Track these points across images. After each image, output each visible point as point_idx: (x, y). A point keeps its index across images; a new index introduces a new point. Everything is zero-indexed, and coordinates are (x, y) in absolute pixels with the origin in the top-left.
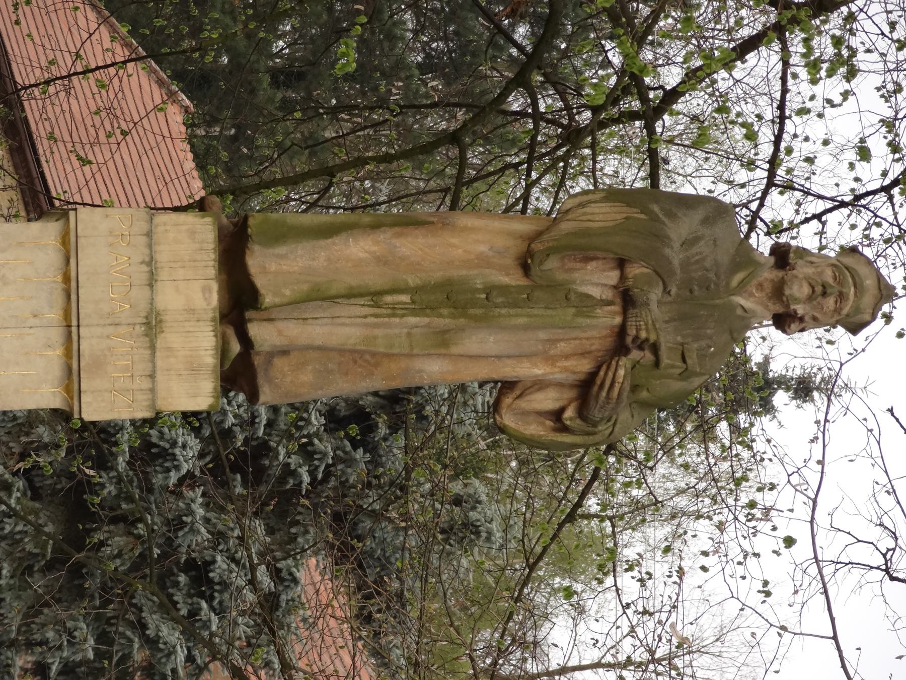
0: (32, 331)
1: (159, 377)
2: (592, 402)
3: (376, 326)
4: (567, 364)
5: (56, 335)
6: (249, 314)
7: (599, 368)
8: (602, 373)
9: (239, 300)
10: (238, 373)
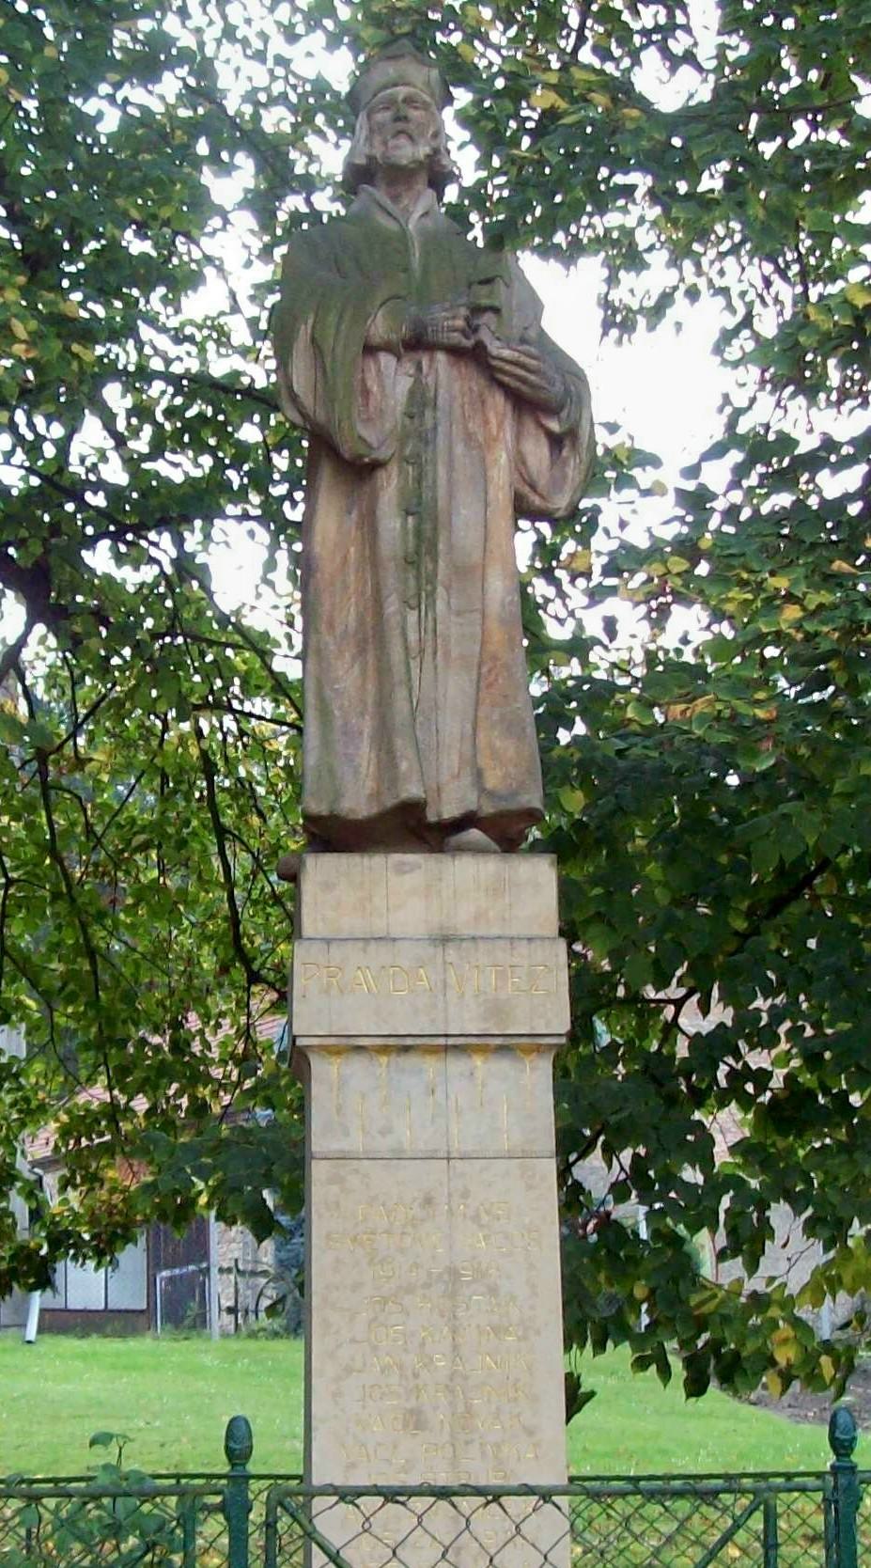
0: (452, 1097)
1: (514, 933)
2: (542, 395)
3: (447, 654)
4: (493, 422)
5: (456, 1065)
6: (431, 817)
7: (501, 385)
8: (506, 379)
9: (412, 828)
10: (506, 833)
